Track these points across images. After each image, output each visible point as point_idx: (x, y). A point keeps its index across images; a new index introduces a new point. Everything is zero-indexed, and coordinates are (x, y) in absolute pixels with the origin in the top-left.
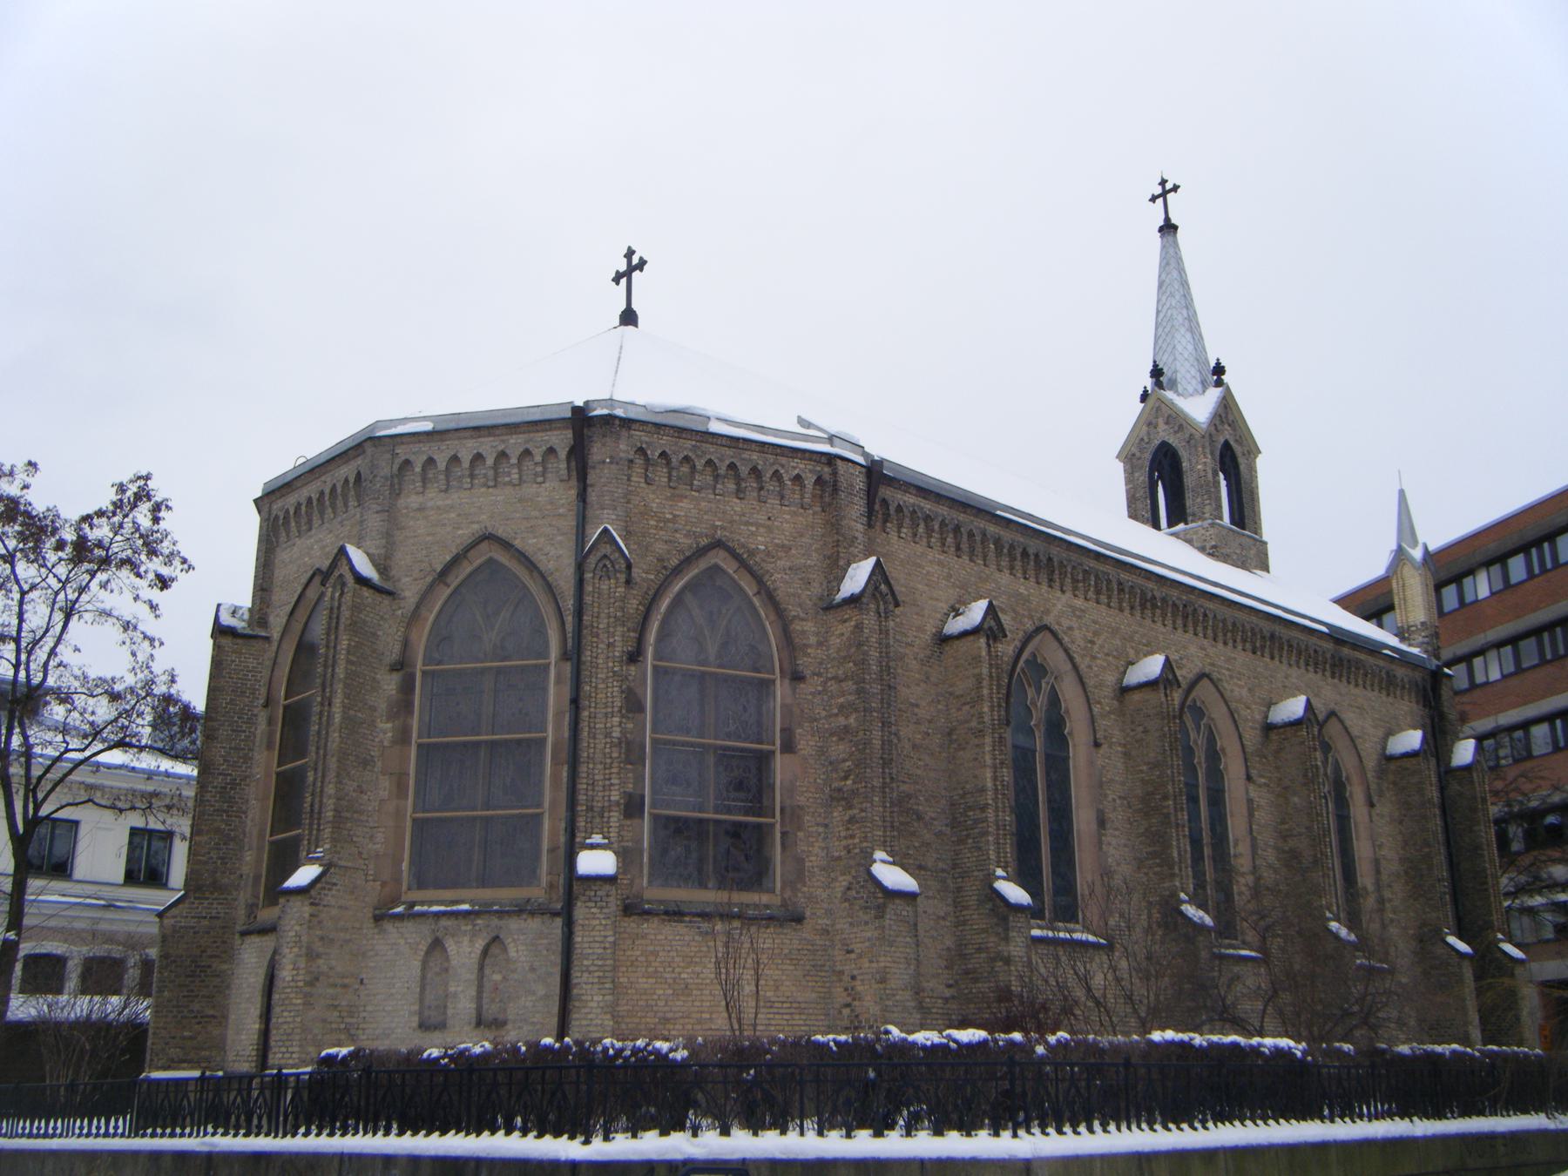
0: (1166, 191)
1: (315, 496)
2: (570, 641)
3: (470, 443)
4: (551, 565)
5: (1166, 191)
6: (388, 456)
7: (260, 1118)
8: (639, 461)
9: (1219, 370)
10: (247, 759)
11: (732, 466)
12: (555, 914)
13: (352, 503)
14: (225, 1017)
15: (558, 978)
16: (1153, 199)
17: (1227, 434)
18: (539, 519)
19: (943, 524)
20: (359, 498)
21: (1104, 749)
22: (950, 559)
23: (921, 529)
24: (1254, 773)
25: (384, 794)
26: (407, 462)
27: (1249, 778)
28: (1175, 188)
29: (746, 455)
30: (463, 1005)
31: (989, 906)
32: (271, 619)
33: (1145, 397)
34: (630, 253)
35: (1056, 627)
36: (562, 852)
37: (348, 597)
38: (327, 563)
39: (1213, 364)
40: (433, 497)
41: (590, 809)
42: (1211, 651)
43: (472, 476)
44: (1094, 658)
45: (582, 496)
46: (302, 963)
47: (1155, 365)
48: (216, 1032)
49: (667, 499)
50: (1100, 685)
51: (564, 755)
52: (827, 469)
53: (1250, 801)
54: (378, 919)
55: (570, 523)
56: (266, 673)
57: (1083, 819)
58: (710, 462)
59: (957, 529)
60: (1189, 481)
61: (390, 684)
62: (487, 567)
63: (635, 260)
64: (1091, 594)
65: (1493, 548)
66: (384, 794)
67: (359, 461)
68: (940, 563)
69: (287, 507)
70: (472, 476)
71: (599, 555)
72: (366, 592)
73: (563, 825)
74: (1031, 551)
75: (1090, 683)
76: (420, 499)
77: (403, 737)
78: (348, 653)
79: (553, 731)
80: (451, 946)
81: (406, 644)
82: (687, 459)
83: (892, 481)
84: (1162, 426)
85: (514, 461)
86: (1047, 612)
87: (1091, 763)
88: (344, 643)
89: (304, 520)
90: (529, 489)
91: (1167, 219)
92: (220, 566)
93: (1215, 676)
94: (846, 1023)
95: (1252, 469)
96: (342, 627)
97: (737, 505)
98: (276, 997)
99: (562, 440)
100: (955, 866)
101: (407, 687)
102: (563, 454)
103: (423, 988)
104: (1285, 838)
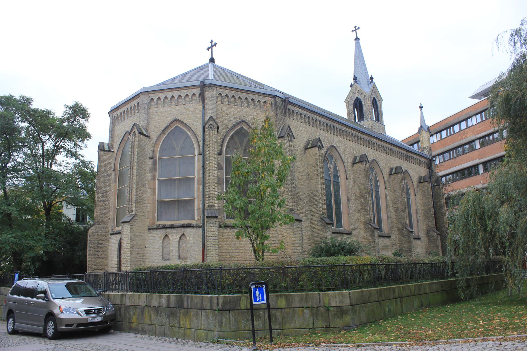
0: (356, 29)
1: (126, 110)
2: (201, 149)
3: (170, 93)
4: (195, 127)
5: (356, 29)
6: (147, 97)
7: (122, 285)
8: (220, 97)
9: (372, 78)
10: (109, 186)
11: (246, 98)
12: (200, 227)
13: (136, 112)
14: (108, 257)
15: (202, 246)
16: (353, 31)
17: (374, 95)
18: (191, 115)
19: (305, 116)
20: (138, 110)
21: (348, 180)
22: (307, 126)
23: (299, 117)
24: (387, 186)
25: (149, 194)
26: (152, 99)
27: (385, 188)
28: (359, 28)
29: (250, 95)
30: (175, 253)
31: (321, 223)
32: (114, 146)
33: (351, 86)
34: (212, 42)
35: (335, 146)
36: (201, 210)
37: (137, 138)
38: (130, 129)
39: (370, 76)
40: (160, 109)
41: (209, 197)
42: (376, 153)
43: (171, 102)
44: (346, 154)
45: (204, 108)
46: (129, 242)
47: (354, 77)
48: (105, 261)
49: (228, 108)
50: (347, 162)
51: (201, 182)
52: (273, 100)
53: (386, 194)
54: (149, 229)
55: (200, 115)
56: (113, 161)
57: (343, 199)
58: (240, 97)
59: (309, 117)
60: (364, 108)
61: (150, 163)
62: (176, 129)
63: (213, 43)
64: (345, 137)
65: (438, 129)
66: (149, 194)
67: (138, 99)
68: (304, 127)
69: (117, 113)
70: (171, 102)
71: (209, 124)
72: (142, 136)
73: (201, 202)
74: (329, 124)
75: (345, 161)
76: (156, 109)
77: (154, 178)
78: (138, 154)
79: (197, 174)
80: (170, 236)
81: (153, 151)
82: (233, 96)
83: (291, 103)
84: (357, 93)
85: (183, 98)
86: (333, 141)
87: (346, 184)
88: (136, 151)
89: (122, 118)
90: (188, 106)
91: (357, 37)
92: (99, 128)
93: (377, 160)
94: (283, 256)
95: (381, 105)
96: (135, 147)
97: (248, 110)
98: (122, 251)
99: (197, 91)
100: (310, 212)
101: (155, 164)
102: (197, 95)
103: (163, 248)
104: (395, 204)
